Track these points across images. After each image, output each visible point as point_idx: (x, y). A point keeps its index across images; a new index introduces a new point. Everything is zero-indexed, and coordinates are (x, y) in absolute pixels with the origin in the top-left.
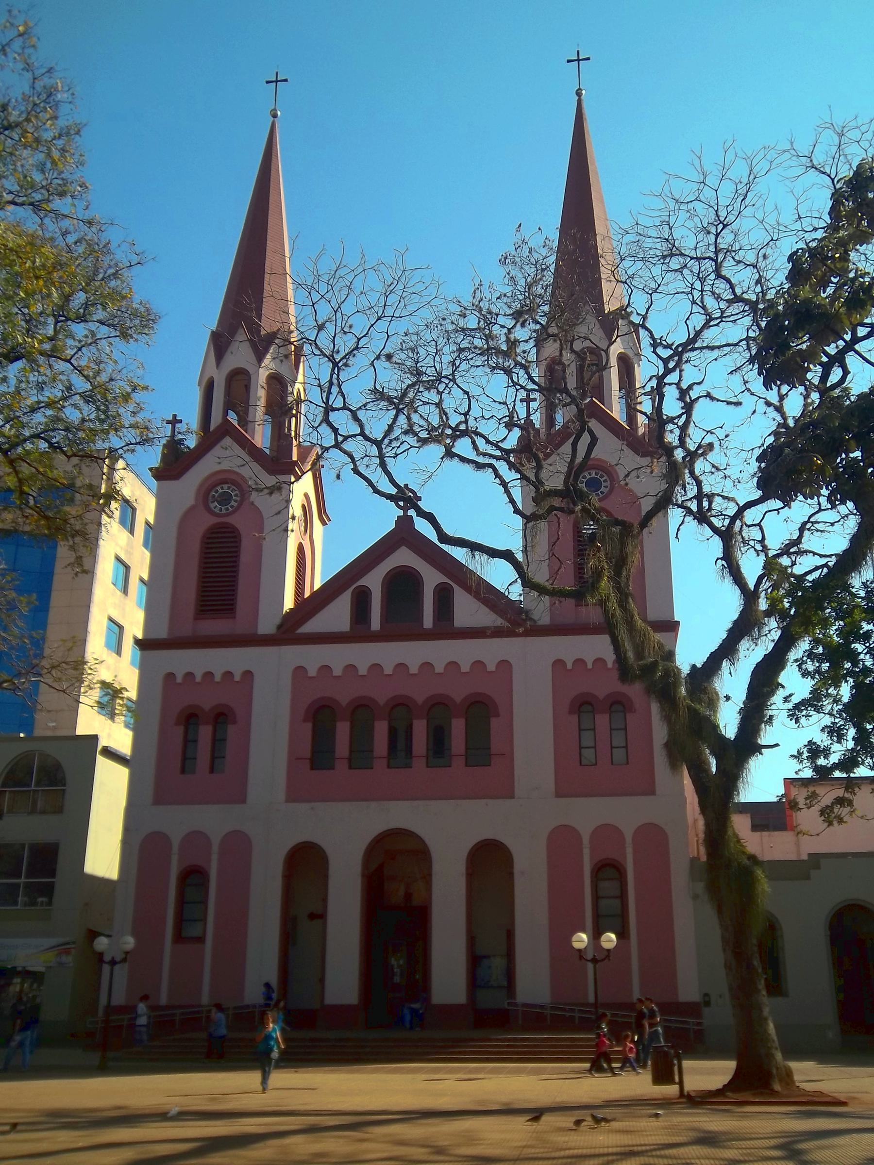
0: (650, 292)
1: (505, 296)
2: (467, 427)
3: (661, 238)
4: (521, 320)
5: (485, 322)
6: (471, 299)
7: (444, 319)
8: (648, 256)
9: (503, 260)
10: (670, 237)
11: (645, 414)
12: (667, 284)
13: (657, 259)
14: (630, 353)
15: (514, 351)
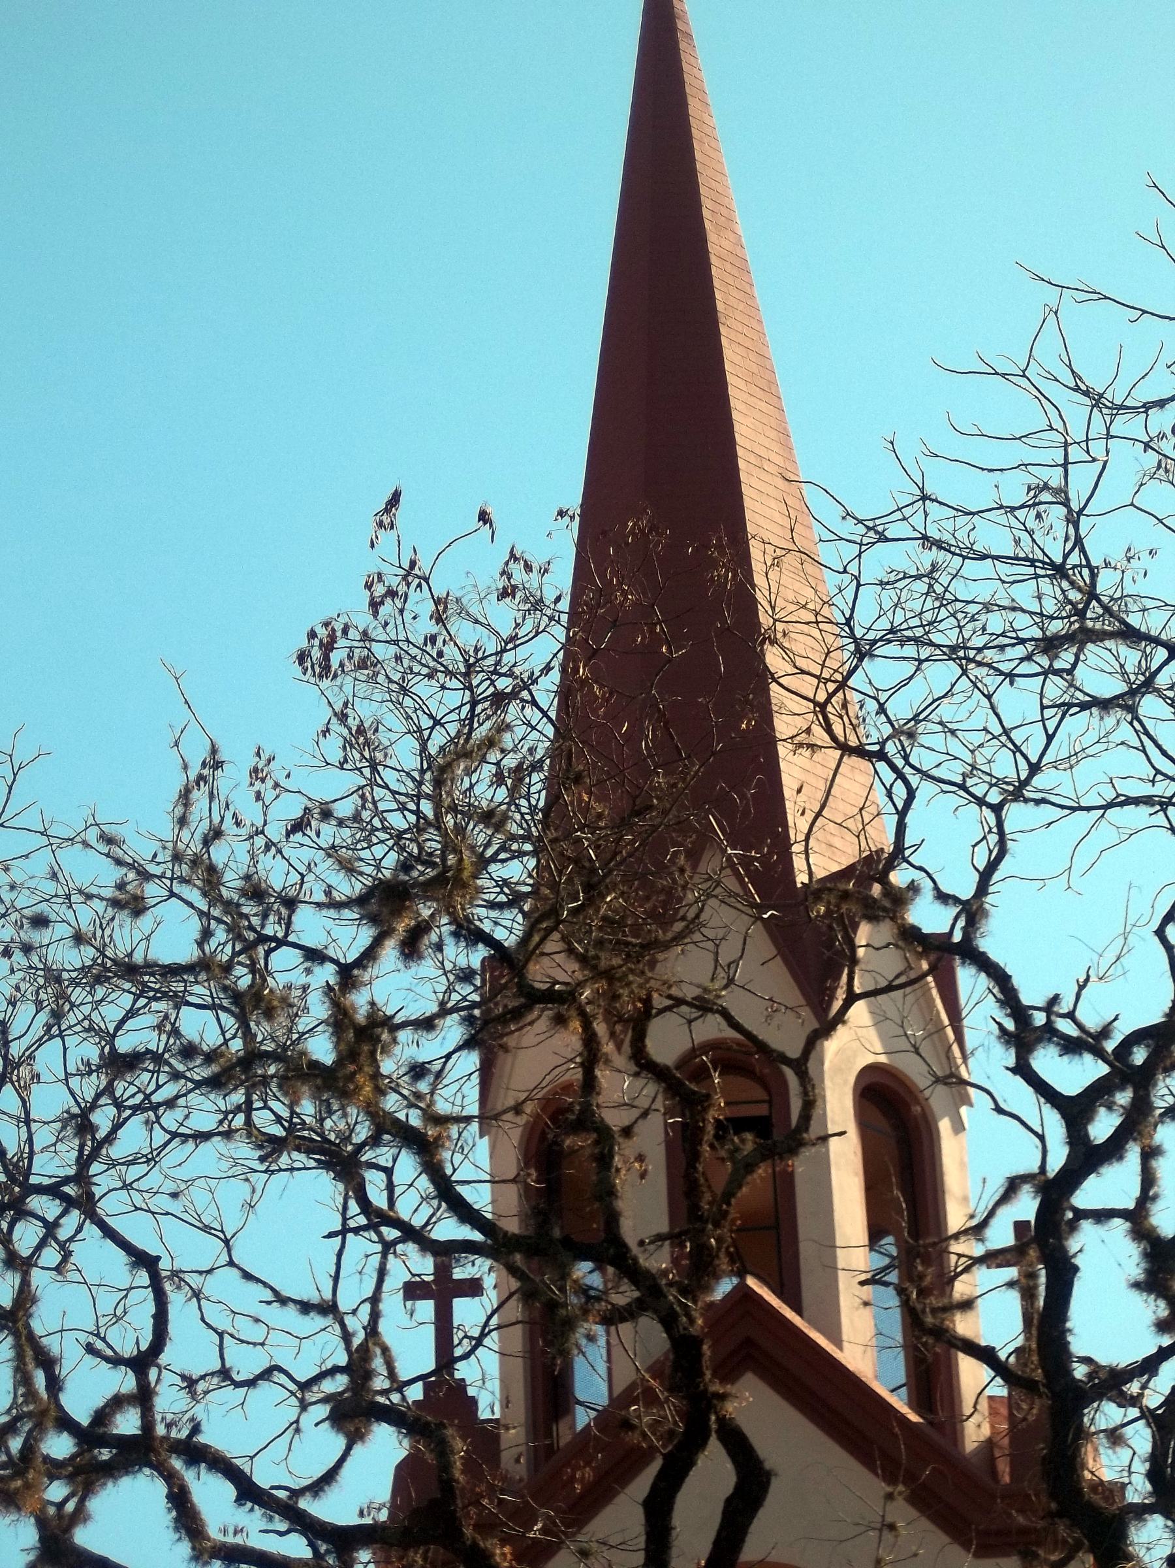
0: (994, 797)
1: (326, 814)
2: (148, 1424)
3: (1032, 562)
4: (402, 926)
5: (234, 932)
6: (167, 830)
7: (40, 922)
8: (978, 641)
9: (316, 653)
10: (1074, 559)
11: (986, 1355)
12: (1071, 761)
13: (1020, 651)
14: (916, 1071)
15: (368, 1070)
